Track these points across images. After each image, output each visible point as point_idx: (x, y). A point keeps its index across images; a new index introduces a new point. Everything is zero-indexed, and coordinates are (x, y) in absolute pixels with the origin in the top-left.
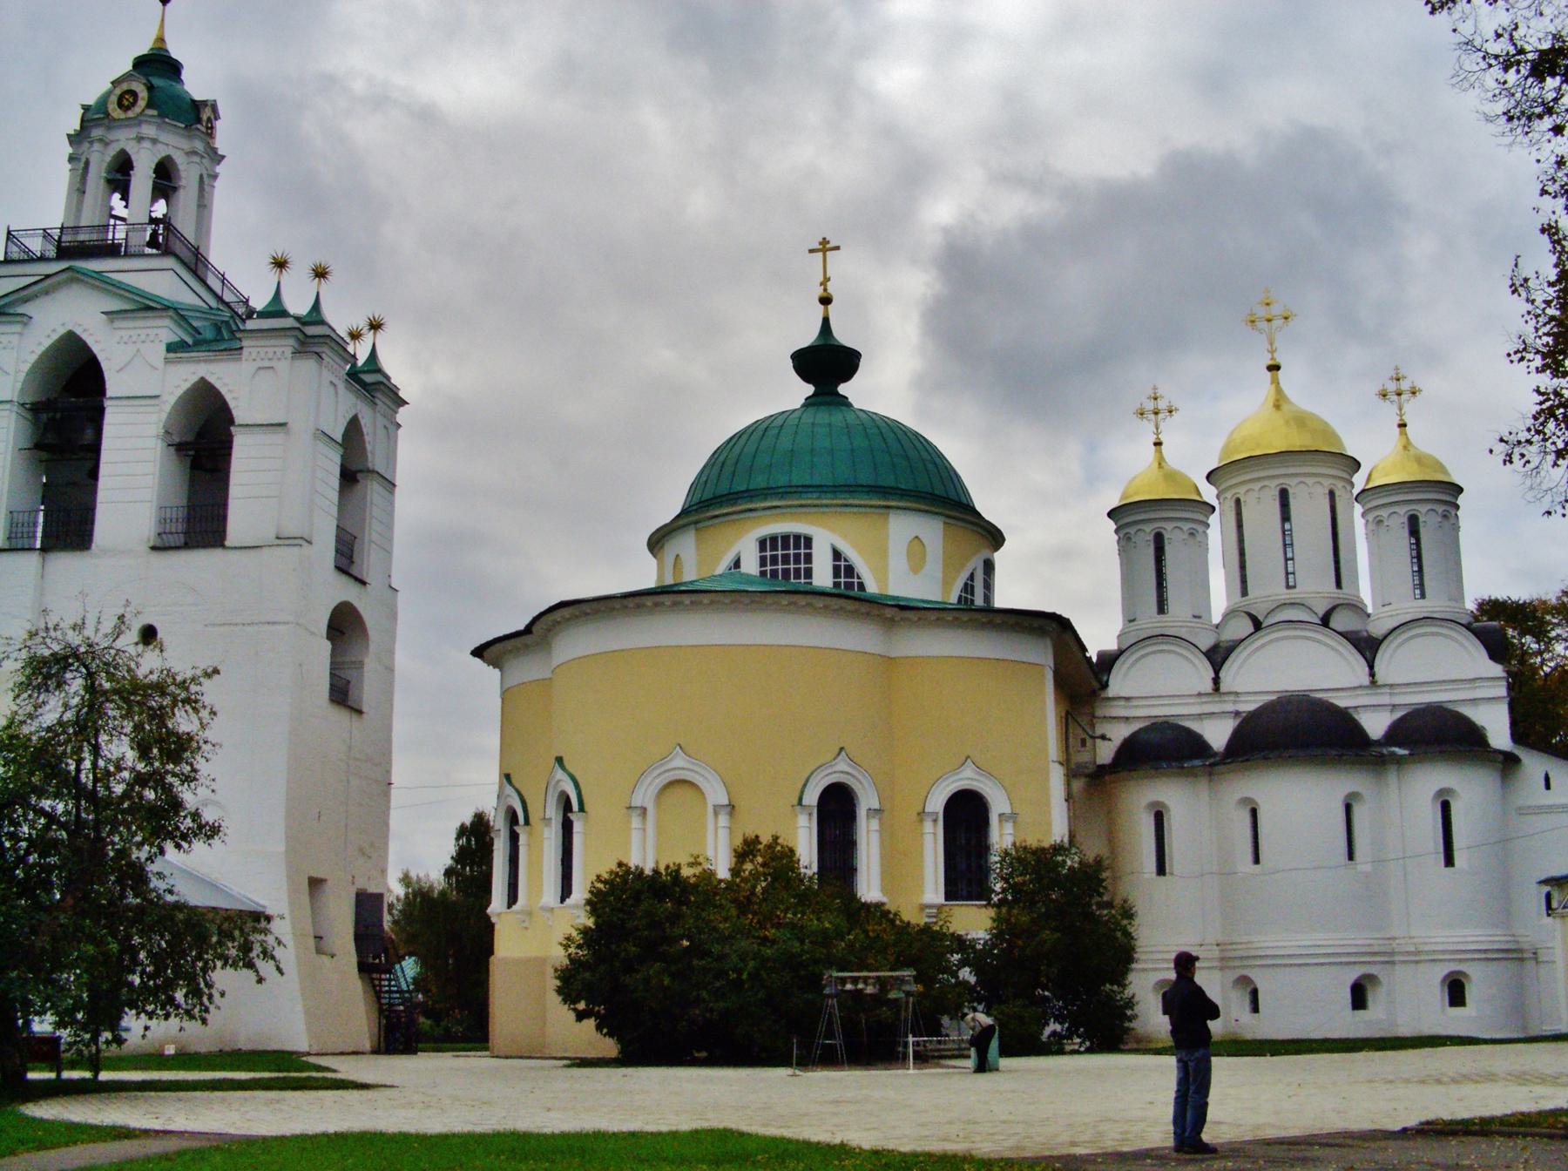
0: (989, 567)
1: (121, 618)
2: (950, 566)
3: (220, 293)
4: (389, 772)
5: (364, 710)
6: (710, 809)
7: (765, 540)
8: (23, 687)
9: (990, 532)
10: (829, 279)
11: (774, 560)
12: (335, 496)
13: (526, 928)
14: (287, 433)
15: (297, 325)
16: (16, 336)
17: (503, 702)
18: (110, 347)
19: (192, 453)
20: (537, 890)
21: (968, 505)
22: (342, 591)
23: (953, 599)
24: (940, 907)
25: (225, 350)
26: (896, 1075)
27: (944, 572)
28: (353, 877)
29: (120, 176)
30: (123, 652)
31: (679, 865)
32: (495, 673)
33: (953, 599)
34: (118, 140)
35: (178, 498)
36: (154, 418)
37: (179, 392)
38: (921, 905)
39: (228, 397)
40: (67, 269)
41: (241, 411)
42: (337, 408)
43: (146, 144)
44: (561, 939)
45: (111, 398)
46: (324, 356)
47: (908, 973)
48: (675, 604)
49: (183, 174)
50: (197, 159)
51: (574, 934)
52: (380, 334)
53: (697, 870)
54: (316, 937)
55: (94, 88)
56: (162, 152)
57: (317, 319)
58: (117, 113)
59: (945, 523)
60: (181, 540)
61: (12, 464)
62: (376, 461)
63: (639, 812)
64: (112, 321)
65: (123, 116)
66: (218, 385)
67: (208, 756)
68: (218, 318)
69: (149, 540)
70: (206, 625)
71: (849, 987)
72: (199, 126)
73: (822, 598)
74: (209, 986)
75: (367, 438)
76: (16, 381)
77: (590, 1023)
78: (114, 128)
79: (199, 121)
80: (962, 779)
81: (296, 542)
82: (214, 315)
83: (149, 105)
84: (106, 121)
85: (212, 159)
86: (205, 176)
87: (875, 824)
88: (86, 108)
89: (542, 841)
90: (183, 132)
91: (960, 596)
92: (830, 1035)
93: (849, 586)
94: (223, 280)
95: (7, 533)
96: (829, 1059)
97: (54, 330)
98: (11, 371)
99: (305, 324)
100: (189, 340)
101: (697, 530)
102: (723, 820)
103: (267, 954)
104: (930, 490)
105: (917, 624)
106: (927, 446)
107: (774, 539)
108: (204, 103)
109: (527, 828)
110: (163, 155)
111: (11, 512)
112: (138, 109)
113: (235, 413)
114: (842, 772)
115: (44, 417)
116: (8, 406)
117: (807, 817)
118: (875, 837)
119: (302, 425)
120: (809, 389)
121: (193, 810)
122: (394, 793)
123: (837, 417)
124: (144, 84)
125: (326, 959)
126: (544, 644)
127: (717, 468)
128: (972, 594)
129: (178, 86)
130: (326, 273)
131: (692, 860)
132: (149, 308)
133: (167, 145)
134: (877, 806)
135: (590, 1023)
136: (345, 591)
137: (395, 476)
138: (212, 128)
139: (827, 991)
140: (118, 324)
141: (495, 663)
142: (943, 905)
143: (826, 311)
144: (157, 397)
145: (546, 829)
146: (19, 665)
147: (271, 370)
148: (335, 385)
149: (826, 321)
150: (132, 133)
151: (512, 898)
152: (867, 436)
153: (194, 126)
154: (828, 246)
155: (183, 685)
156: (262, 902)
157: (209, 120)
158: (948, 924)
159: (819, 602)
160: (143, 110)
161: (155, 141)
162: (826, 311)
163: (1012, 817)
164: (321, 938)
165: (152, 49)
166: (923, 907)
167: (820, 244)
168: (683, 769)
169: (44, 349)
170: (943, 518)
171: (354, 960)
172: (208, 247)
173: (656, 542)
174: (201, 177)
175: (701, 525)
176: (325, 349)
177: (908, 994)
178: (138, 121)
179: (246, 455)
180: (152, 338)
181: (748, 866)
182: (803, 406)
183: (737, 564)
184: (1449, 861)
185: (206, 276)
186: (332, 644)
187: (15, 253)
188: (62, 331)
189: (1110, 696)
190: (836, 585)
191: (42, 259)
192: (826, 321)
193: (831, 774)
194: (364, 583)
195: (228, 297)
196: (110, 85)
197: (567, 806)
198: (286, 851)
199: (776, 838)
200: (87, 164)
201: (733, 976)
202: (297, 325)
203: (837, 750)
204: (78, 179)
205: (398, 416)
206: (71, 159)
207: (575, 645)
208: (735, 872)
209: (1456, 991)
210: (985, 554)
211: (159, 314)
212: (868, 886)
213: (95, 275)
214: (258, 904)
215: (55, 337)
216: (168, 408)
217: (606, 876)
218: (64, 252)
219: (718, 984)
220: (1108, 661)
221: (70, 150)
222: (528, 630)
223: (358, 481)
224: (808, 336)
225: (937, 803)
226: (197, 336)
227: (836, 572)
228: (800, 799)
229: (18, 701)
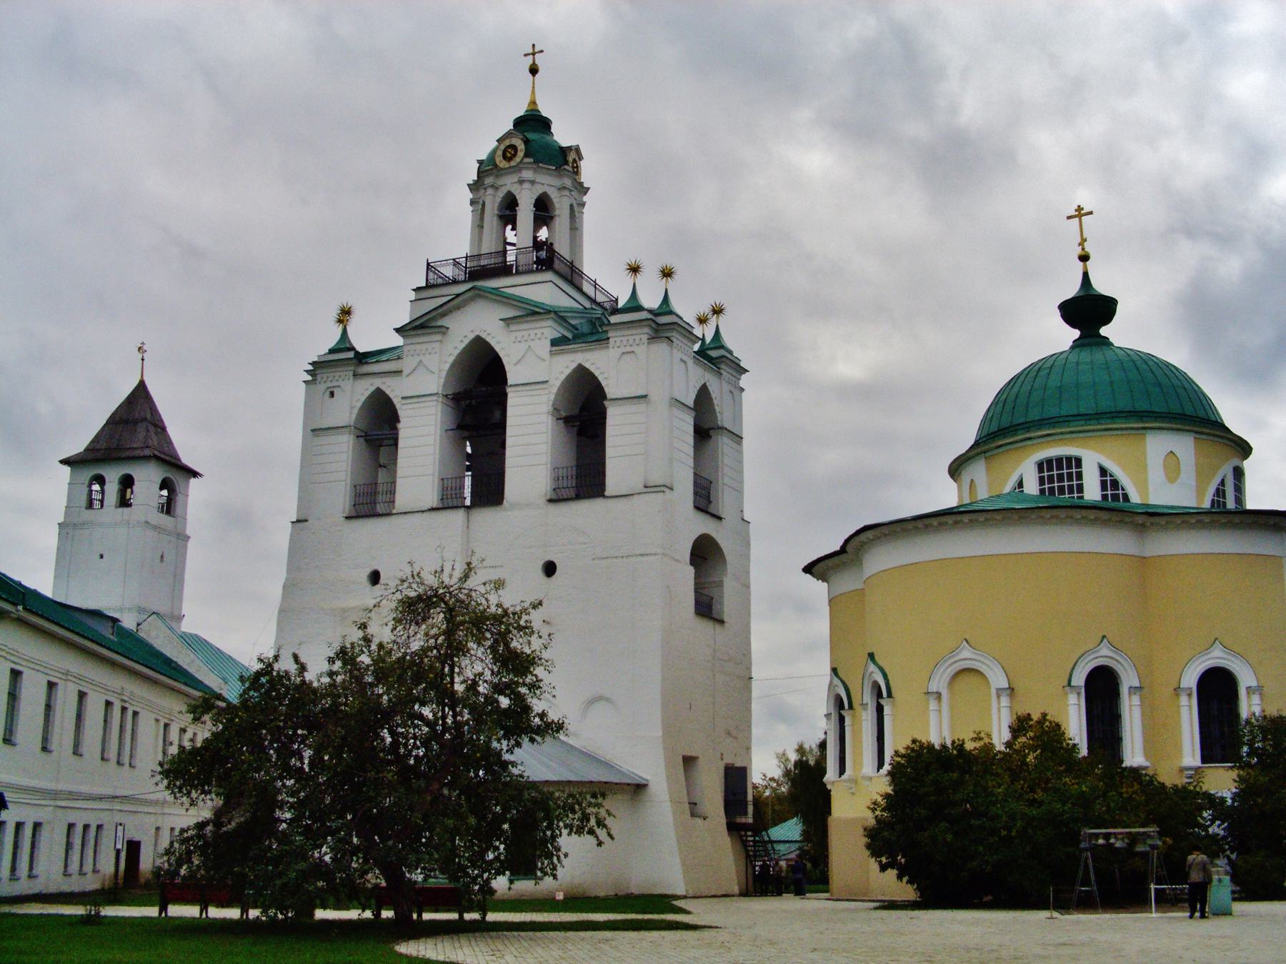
0: (1239, 474)
1: (469, 564)
2: (1202, 475)
3: (593, 296)
4: (749, 669)
5: (725, 620)
6: (993, 692)
7: (1043, 463)
8: (398, 621)
9: (1239, 445)
10: (1085, 240)
11: (1051, 479)
12: (691, 451)
13: (853, 794)
14: (648, 403)
15: (650, 316)
16: (438, 344)
17: (830, 609)
18: (510, 346)
19: (578, 423)
20: (858, 764)
21: (1217, 422)
22: (700, 525)
23: (1206, 504)
24: (1197, 769)
25: (595, 341)
26: (1078, 922)
27: (1197, 481)
28: (722, 754)
29: (508, 212)
30: (475, 591)
31: (963, 740)
34: (506, 185)
35: (568, 460)
36: (545, 398)
37: (563, 377)
38: (1180, 767)
39: (600, 378)
40: (472, 288)
41: (612, 388)
42: (685, 381)
43: (526, 185)
44: (869, 803)
45: (511, 386)
46: (674, 340)
47: (1151, 829)
48: (956, 523)
49: (557, 206)
50: (567, 193)
51: (880, 799)
52: (722, 317)
53: (978, 744)
54: (690, 803)
55: (485, 146)
56: (539, 190)
57: (667, 309)
58: (503, 164)
59: (1195, 438)
60: (572, 493)
61: (441, 443)
62: (724, 418)
63: (935, 696)
64: (508, 325)
65: (507, 166)
66: (592, 369)
67: (550, 669)
68: (594, 316)
69: (546, 494)
70: (594, 559)
71: (1101, 841)
72: (566, 167)
73: (1093, 511)
74: (558, 849)
75: (715, 402)
76: (439, 377)
77: (892, 873)
78: (501, 175)
79: (566, 163)
80: (1213, 658)
81: (659, 489)
82: (589, 313)
83: (526, 155)
84: (495, 171)
85: (580, 192)
86: (575, 205)
87: (1136, 700)
88: (481, 162)
89: (861, 722)
90: (554, 173)
92: (1086, 882)
93: (1115, 498)
94: (595, 284)
95: (440, 494)
96: (1086, 904)
97: (466, 336)
98: (435, 370)
100: (569, 335)
101: (986, 458)
102: (1005, 701)
103: (600, 823)
104: (1181, 411)
105: (1164, 528)
106: (1177, 374)
107: (1049, 461)
108: (570, 148)
109: (851, 711)
110: (541, 192)
111: (442, 479)
112: (518, 159)
113: (606, 390)
114: (1106, 657)
115: (463, 403)
116: (435, 398)
117: (1076, 696)
118: (1137, 713)
119: (659, 397)
120: (1076, 333)
121: (540, 711)
122: (754, 684)
123: (1098, 355)
125: (699, 821)
126: (857, 561)
127: (1000, 405)
128: (1224, 497)
129: (548, 138)
130: (672, 273)
131: (975, 736)
132: (535, 313)
133: (543, 184)
134: (1138, 685)
135: (892, 873)
136: (703, 525)
137: (742, 432)
138: (577, 167)
139: (1083, 845)
140: (513, 327)
141: (822, 577)
142: (1200, 767)
144: (547, 382)
146: (394, 605)
147: (631, 356)
148: (685, 362)
149: (1086, 275)
150: (515, 178)
151: (842, 770)
152: (1124, 370)
153: (562, 168)
154: (1082, 212)
155: (517, 616)
156: (645, 777)
157: (574, 161)
158: (1201, 784)
159: (1092, 514)
160: (522, 159)
161: (533, 182)
162: (1085, 267)
163: (1259, 690)
164: (695, 804)
165: (526, 111)
166: (1182, 770)
167: (1076, 211)
168: (970, 659)
169: (459, 351)
170: (1193, 434)
171: (723, 820)
172: (581, 258)
173: (956, 469)
174: (571, 206)
175: (987, 454)
176: (674, 334)
177: (1153, 847)
178: (518, 168)
179: (618, 424)
180: (539, 336)
181: (1022, 739)
182: (1073, 348)
183: (1020, 484)
185: (582, 284)
186: (695, 568)
188: (471, 336)
190: (1104, 497)
191: (455, 282)
192: (1086, 275)
193: (1097, 658)
194: (720, 518)
195: (600, 298)
196: (497, 143)
197: (879, 695)
198: (663, 735)
199: (1044, 715)
200: (484, 205)
201: (1004, 833)
202: (650, 316)
204: (479, 217)
205: (741, 381)
206: (472, 202)
207: (881, 560)
208: (1009, 744)
210: (1235, 462)
211: (542, 317)
212: (1133, 752)
213: (494, 292)
214: (643, 779)
215: (467, 341)
216: (555, 390)
217: (903, 751)
219: (991, 840)
221: (471, 196)
222: (843, 550)
223: (711, 437)
224: (1071, 289)
225: (1190, 679)
226: (576, 332)
227: (1104, 486)
228: (1070, 681)
229: (395, 633)
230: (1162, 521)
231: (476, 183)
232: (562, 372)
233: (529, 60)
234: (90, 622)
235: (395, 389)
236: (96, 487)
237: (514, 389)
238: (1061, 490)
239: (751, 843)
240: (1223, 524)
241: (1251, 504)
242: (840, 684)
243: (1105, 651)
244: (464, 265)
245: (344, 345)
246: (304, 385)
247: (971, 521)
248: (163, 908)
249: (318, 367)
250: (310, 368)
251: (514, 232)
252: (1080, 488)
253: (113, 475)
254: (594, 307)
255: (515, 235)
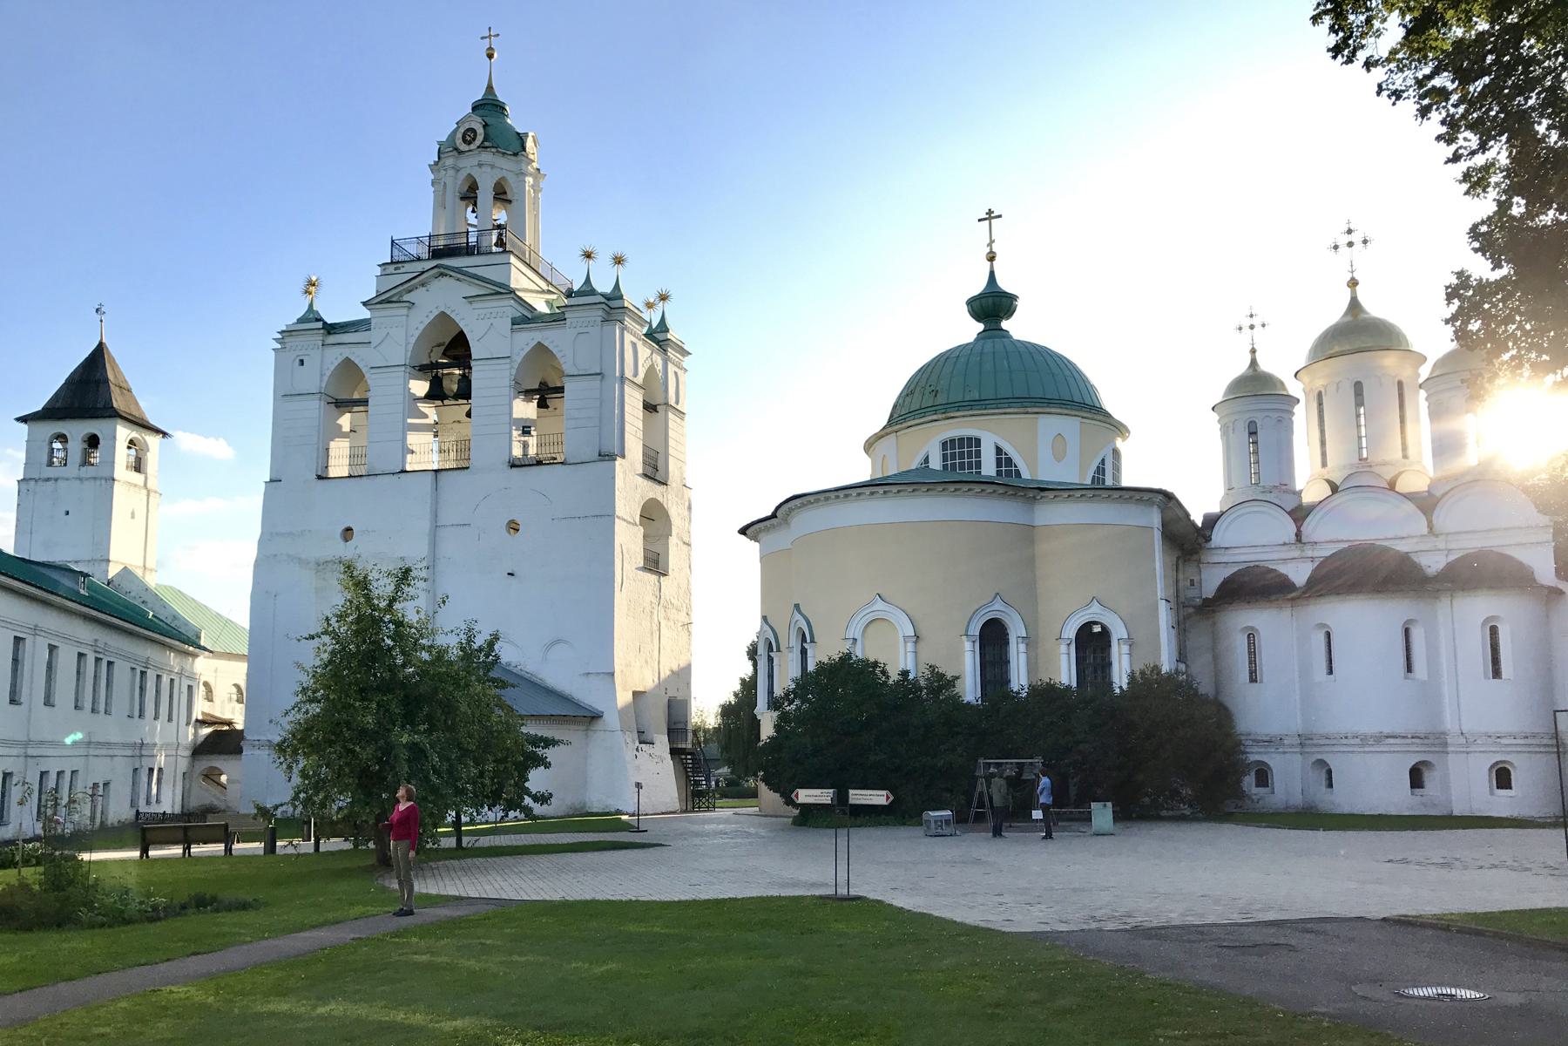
15: (603, 300)
32: (756, 546)
33: (1088, 481)
56: (497, 176)
76: (406, 351)
87: (1022, 647)
88: (440, 143)
91: (1094, 476)
99: (609, 299)
107: (952, 441)
116: (403, 369)
118: (1023, 657)
120: (980, 327)
124: (481, 123)
140: (475, 305)
141: (755, 538)
143: (992, 266)
145: (790, 654)
149: (992, 274)
161: (493, 166)
162: (992, 266)
167: (987, 214)
170: (1080, 418)
173: (869, 446)
183: (926, 460)
184: (1497, 673)
187: (399, 256)
188: (436, 313)
189: (1213, 547)
190: (999, 473)
192: (992, 274)
197: (804, 639)
202: (603, 300)
203: (993, 595)
207: (805, 522)
209: (1503, 778)
218: (436, 254)
220: (1211, 521)
222: (774, 515)
224: (978, 286)
225: (1071, 632)
230: (1051, 495)
231: (436, 163)
232: (523, 349)
233: (486, 43)
234: (55, 575)
235: (360, 357)
236: (57, 445)
237: (479, 362)
238: (962, 466)
239: (704, 783)
240: (1000, 494)
241: (1125, 482)
242: (769, 629)
243: (998, 605)
244: (427, 244)
245: (311, 316)
246: (273, 353)
247: (885, 492)
248: (145, 851)
249: (287, 333)
250: (279, 336)
251: (475, 214)
252: (979, 465)
253: (77, 430)
254: (551, 289)
255: (476, 217)
